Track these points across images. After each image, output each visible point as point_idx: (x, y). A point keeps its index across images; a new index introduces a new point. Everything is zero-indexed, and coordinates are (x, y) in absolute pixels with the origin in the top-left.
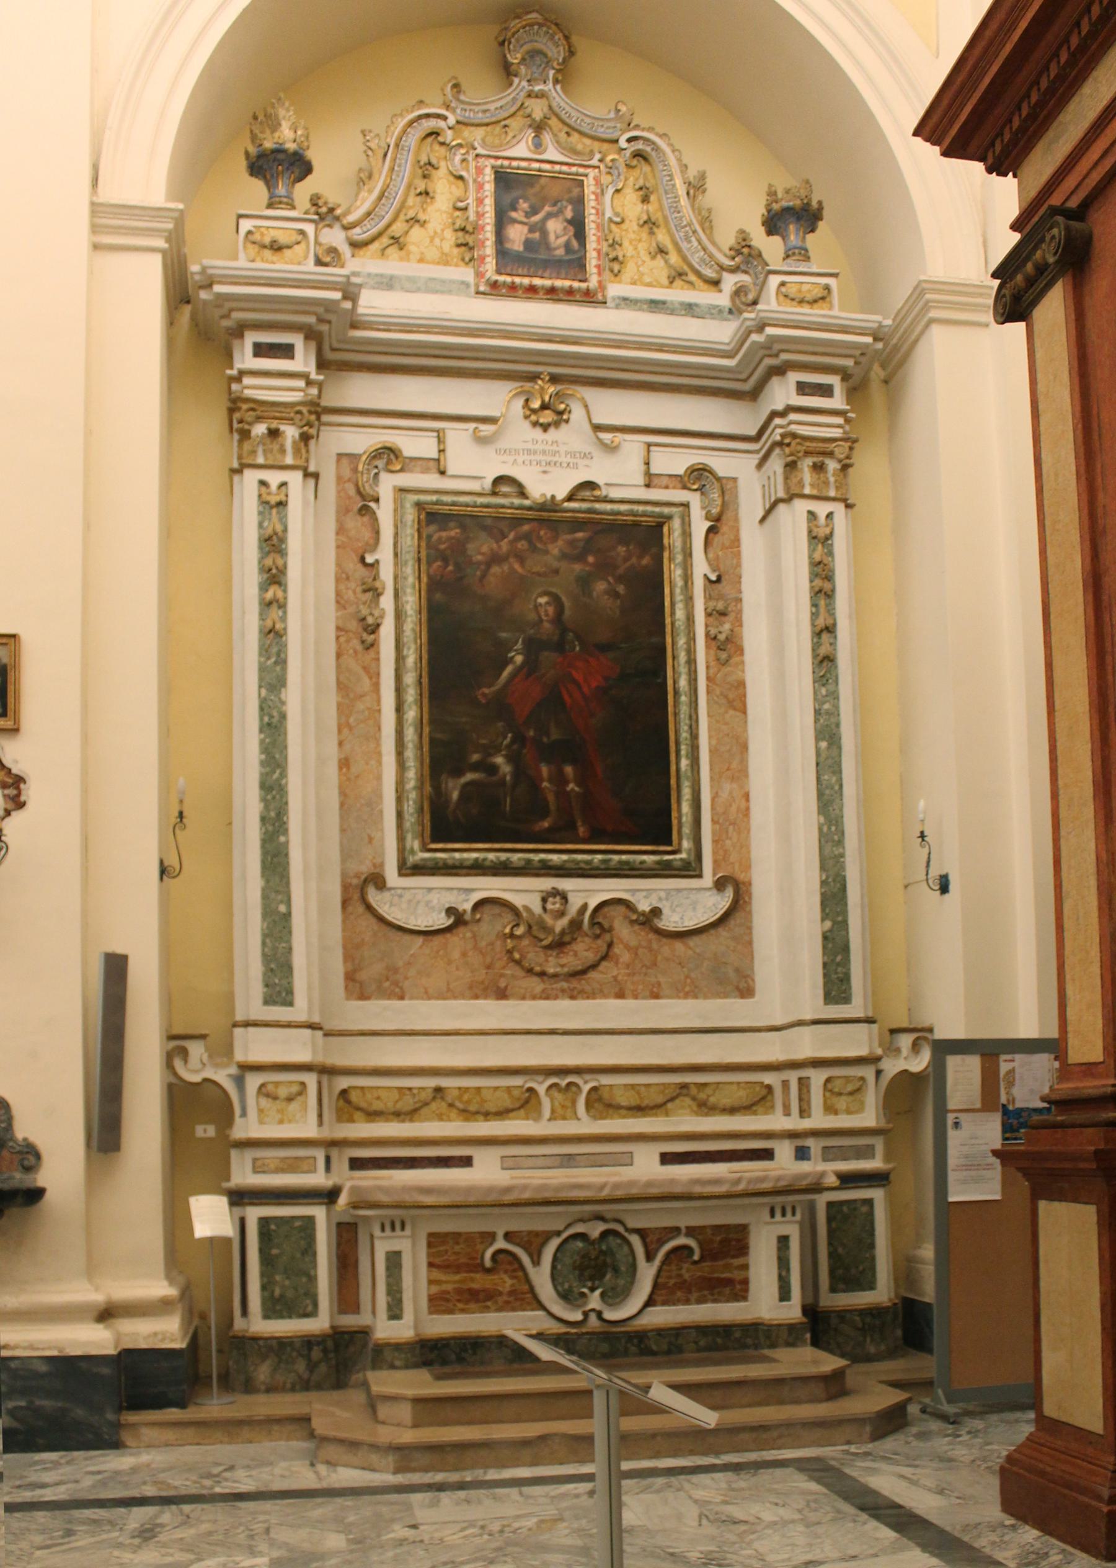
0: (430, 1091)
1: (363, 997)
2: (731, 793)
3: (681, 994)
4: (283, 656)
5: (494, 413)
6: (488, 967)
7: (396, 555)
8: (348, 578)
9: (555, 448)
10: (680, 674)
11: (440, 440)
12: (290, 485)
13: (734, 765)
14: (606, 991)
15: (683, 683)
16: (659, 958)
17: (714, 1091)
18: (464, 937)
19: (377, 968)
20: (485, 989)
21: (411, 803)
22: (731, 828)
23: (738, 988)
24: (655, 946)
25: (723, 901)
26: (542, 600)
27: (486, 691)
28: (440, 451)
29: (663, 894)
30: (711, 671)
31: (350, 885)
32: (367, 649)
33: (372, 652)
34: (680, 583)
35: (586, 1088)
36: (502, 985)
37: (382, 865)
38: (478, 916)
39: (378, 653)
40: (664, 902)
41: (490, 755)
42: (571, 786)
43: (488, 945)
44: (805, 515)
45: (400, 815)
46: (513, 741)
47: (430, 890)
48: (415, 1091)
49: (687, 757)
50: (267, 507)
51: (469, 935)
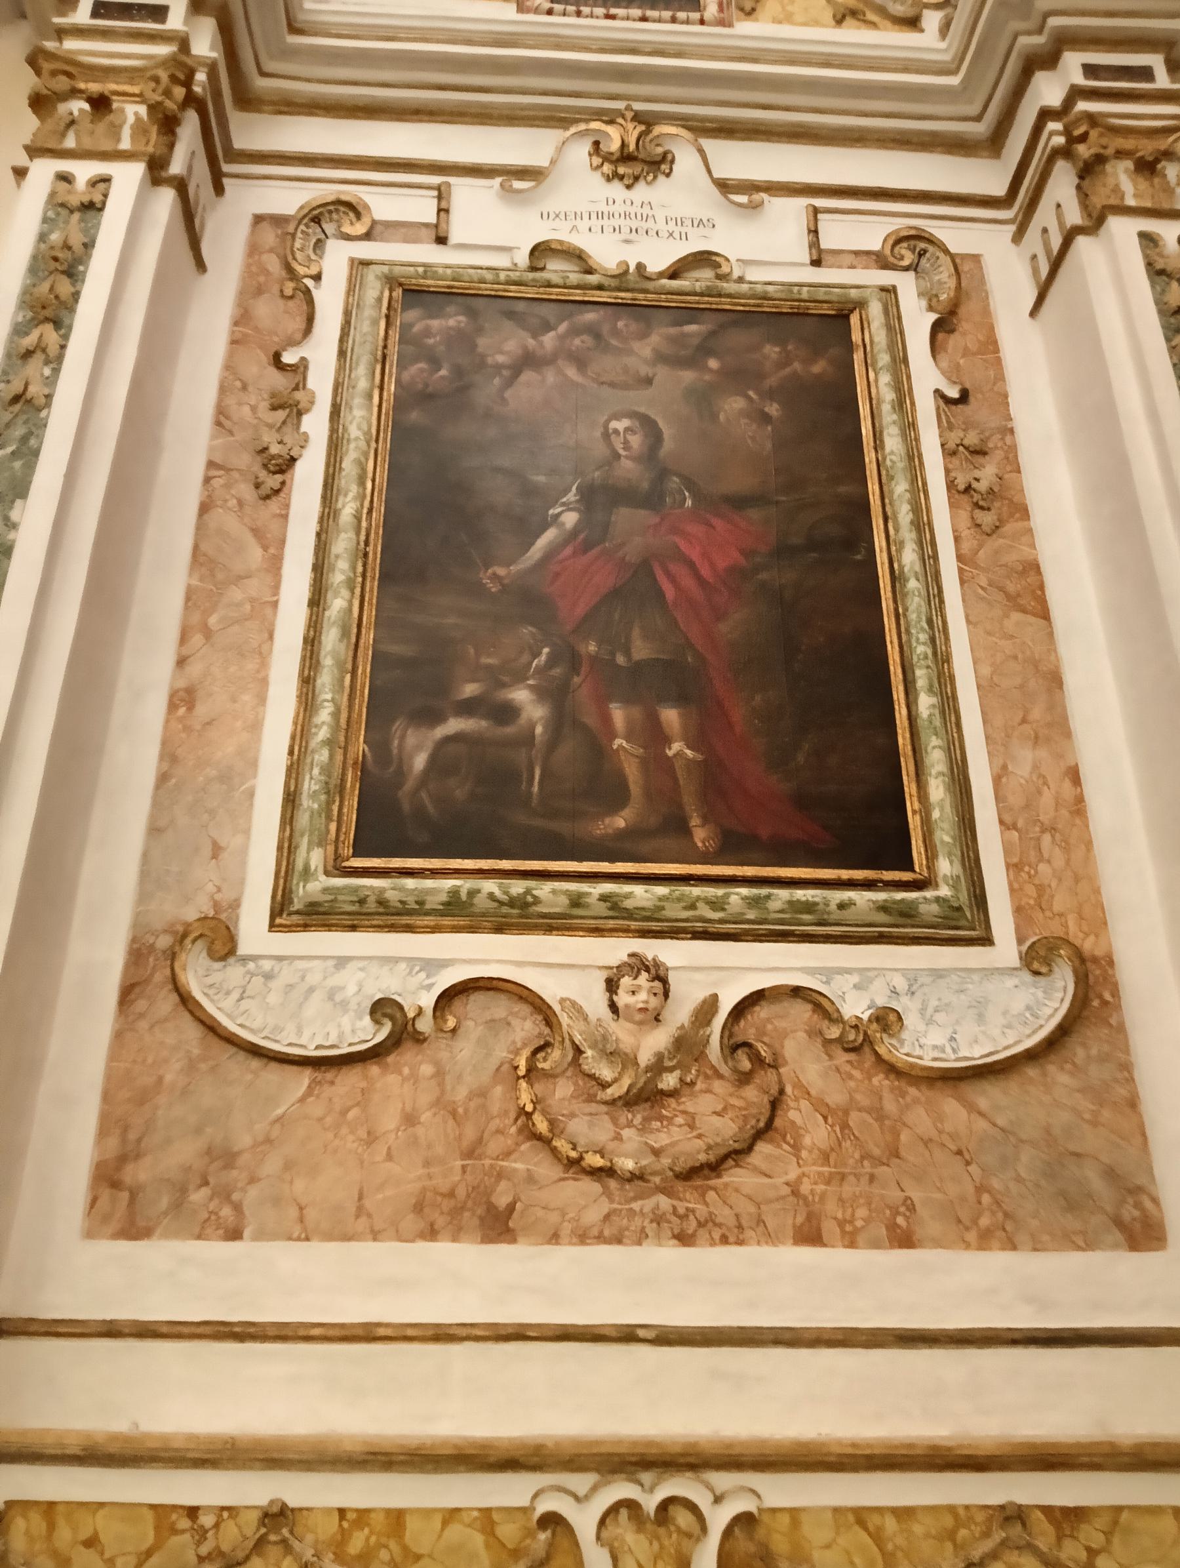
0: (255, 1516)
1: (134, 1229)
2: (1035, 767)
3: (971, 1236)
4: (33, 442)
5: (542, 161)
6: (469, 1154)
7: (342, 353)
8: (244, 387)
9: (646, 210)
10: (901, 545)
11: (442, 194)
12: (114, 183)
13: (1037, 713)
14: (771, 1223)
15: (909, 557)
16: (904, 1137)
17: (1108, 1534)
18: (414, 1077)
19: (183, 1153)
20: (456, 1212)
21: (316, 771)
22: (1047, 839)
23: (1119, 1223)
24: (890, 1105)
25: (1051, 1001)
26: (620, 425)
27: (501, 571)
28: (439, 210)
29: (900, 983)
30: (966, 547)
31: (152, 948)
32: (267, 497)
33: (274, 505)
34: (888, 396)
35: (719, 1519)
36: (502, 1200)
37: (236, 904)
38: (451, 1022)
39: (287, 506)
40: (905, 1000)
41: (504, 685)
42: (676, 746)
43: (471, 1096)
44: (1136, 239)
45: (291, 800)
46: (552, 662)
47: (342, 962)
48: (207, 1520)
49: (930, 690)
50: (64, 212)
51: (427, 1069)
